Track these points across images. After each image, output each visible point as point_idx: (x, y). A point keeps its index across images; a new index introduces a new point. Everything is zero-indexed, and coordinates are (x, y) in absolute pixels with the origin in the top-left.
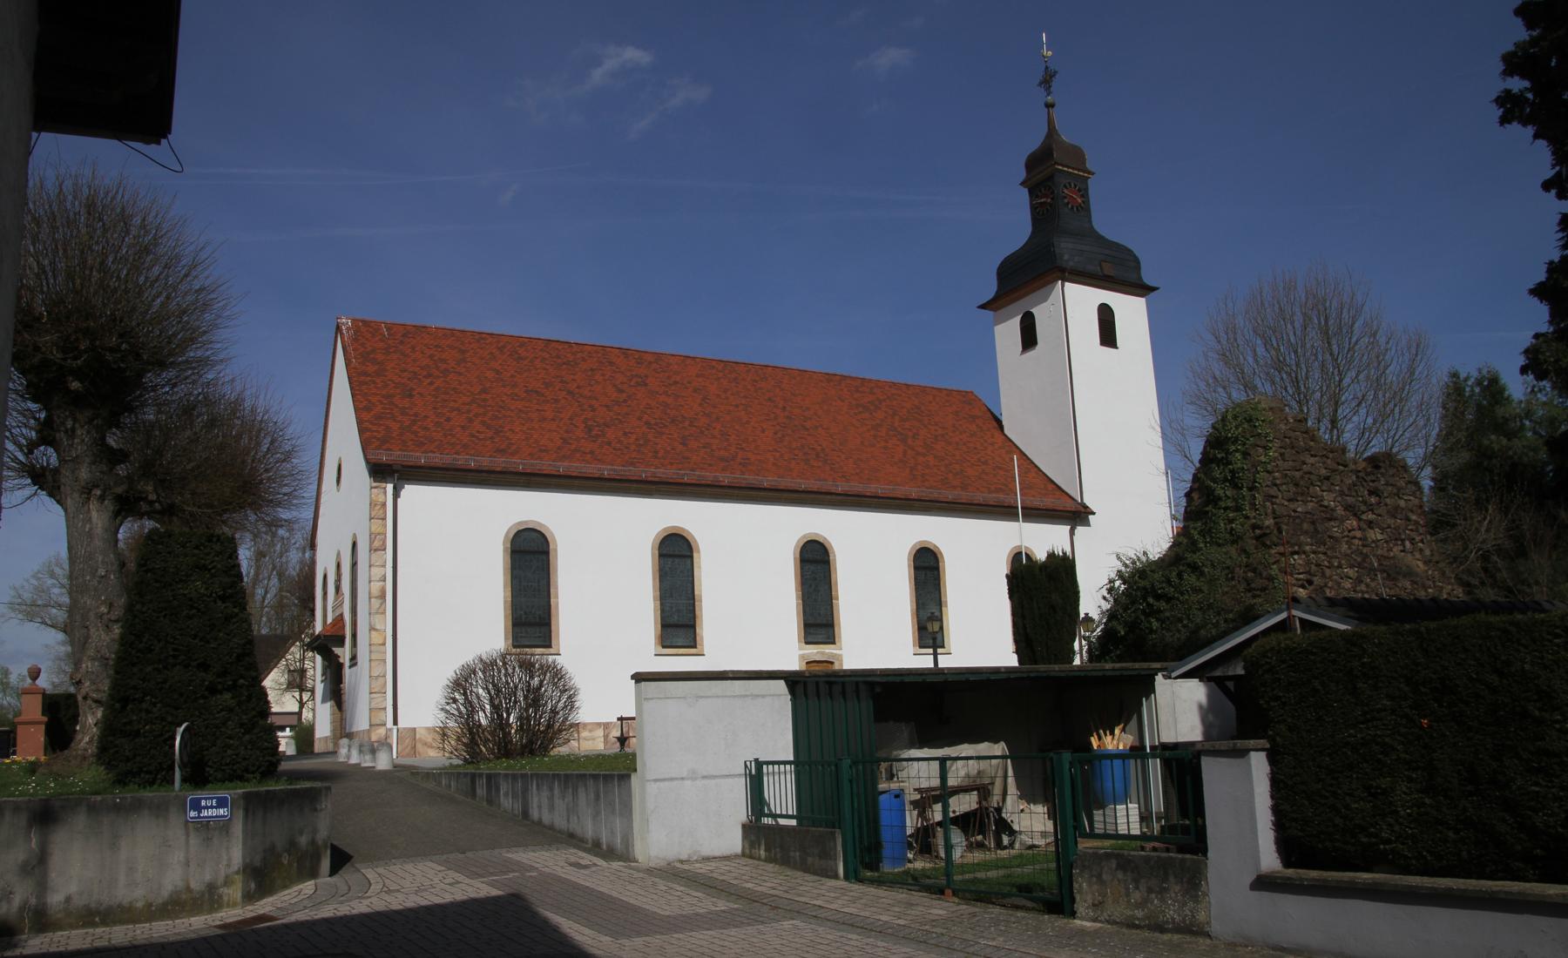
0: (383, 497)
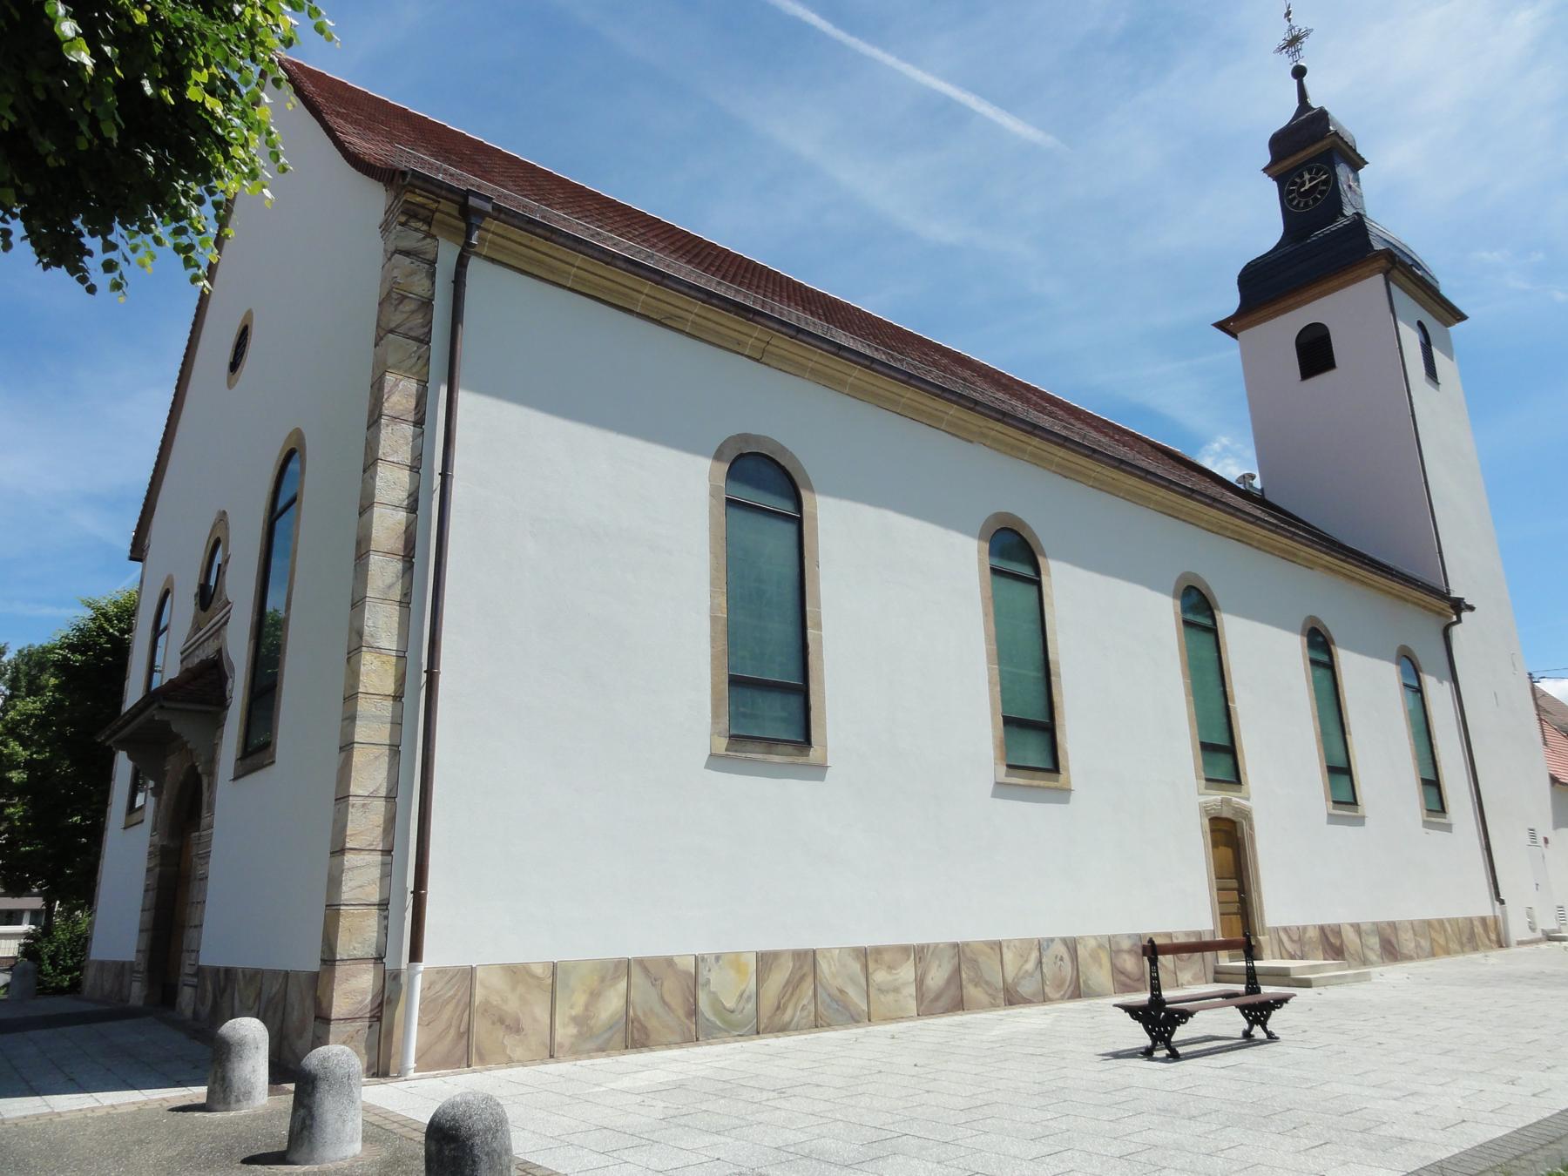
0: (427, 283)
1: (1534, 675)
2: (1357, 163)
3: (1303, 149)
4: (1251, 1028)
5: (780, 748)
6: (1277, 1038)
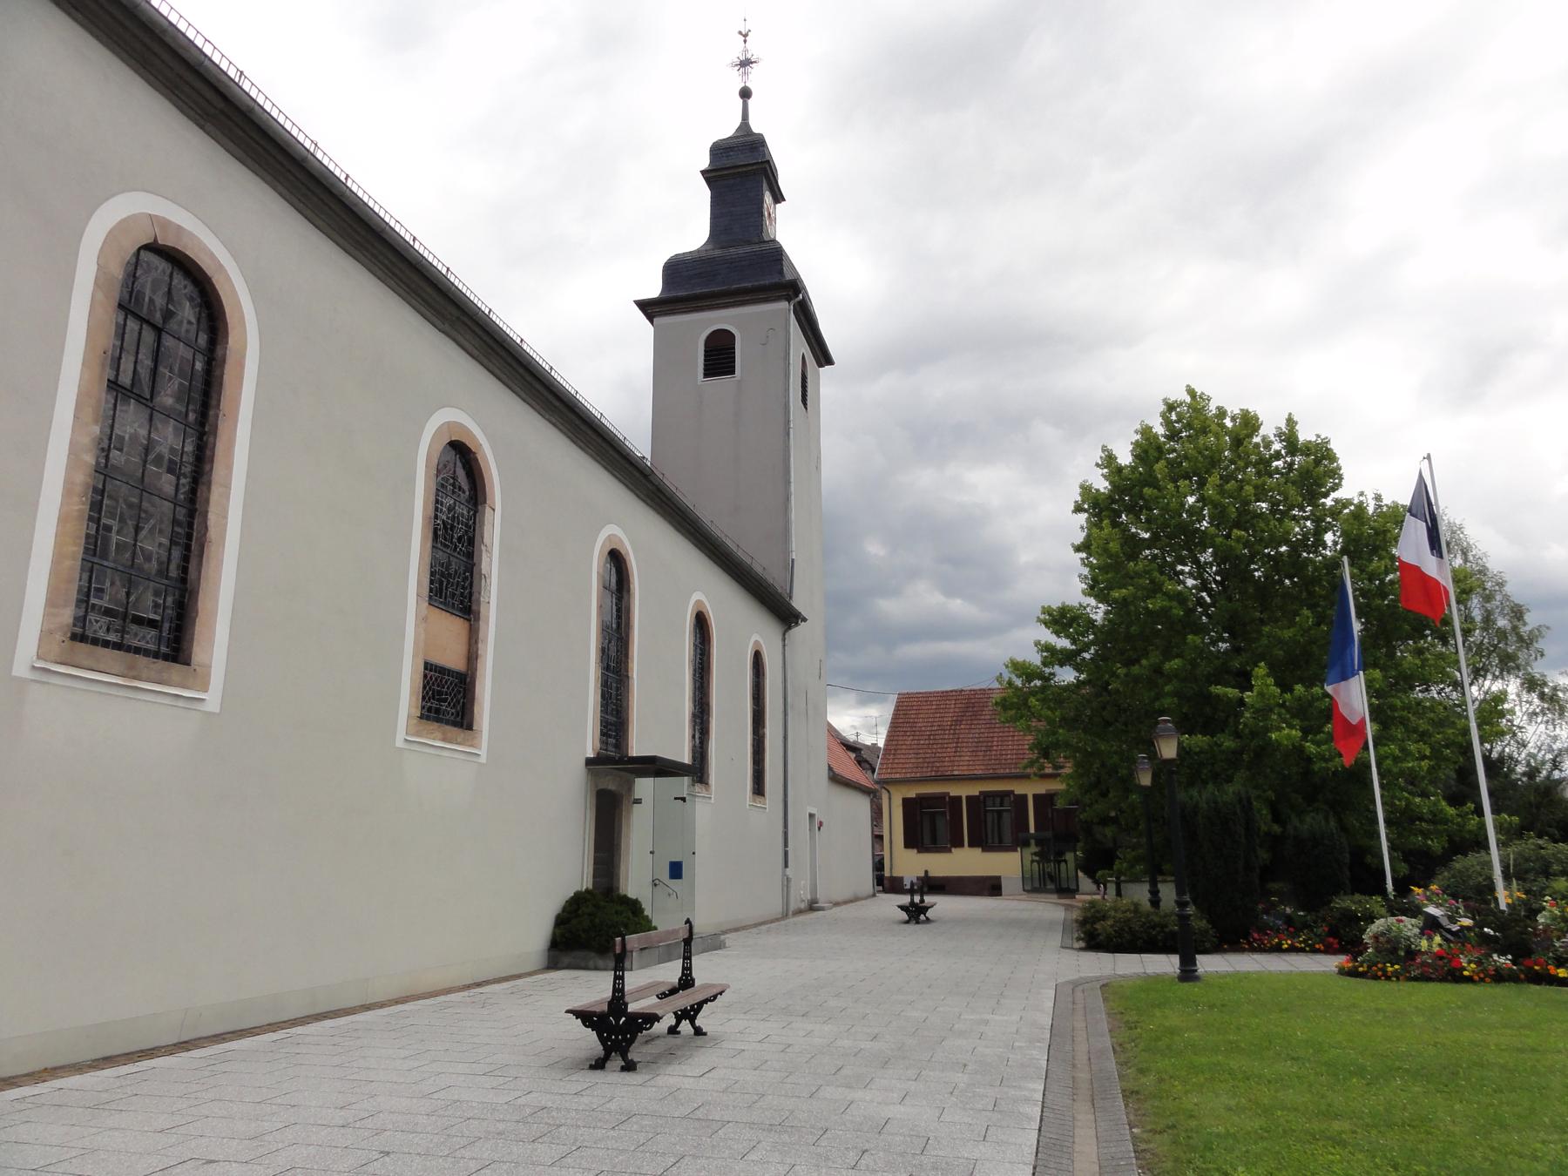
1: (92, 553)
2: (778, 197)
3: (739, 172)
4: (678, 1023)
5: (610, 602)
6: (705, 1034)
